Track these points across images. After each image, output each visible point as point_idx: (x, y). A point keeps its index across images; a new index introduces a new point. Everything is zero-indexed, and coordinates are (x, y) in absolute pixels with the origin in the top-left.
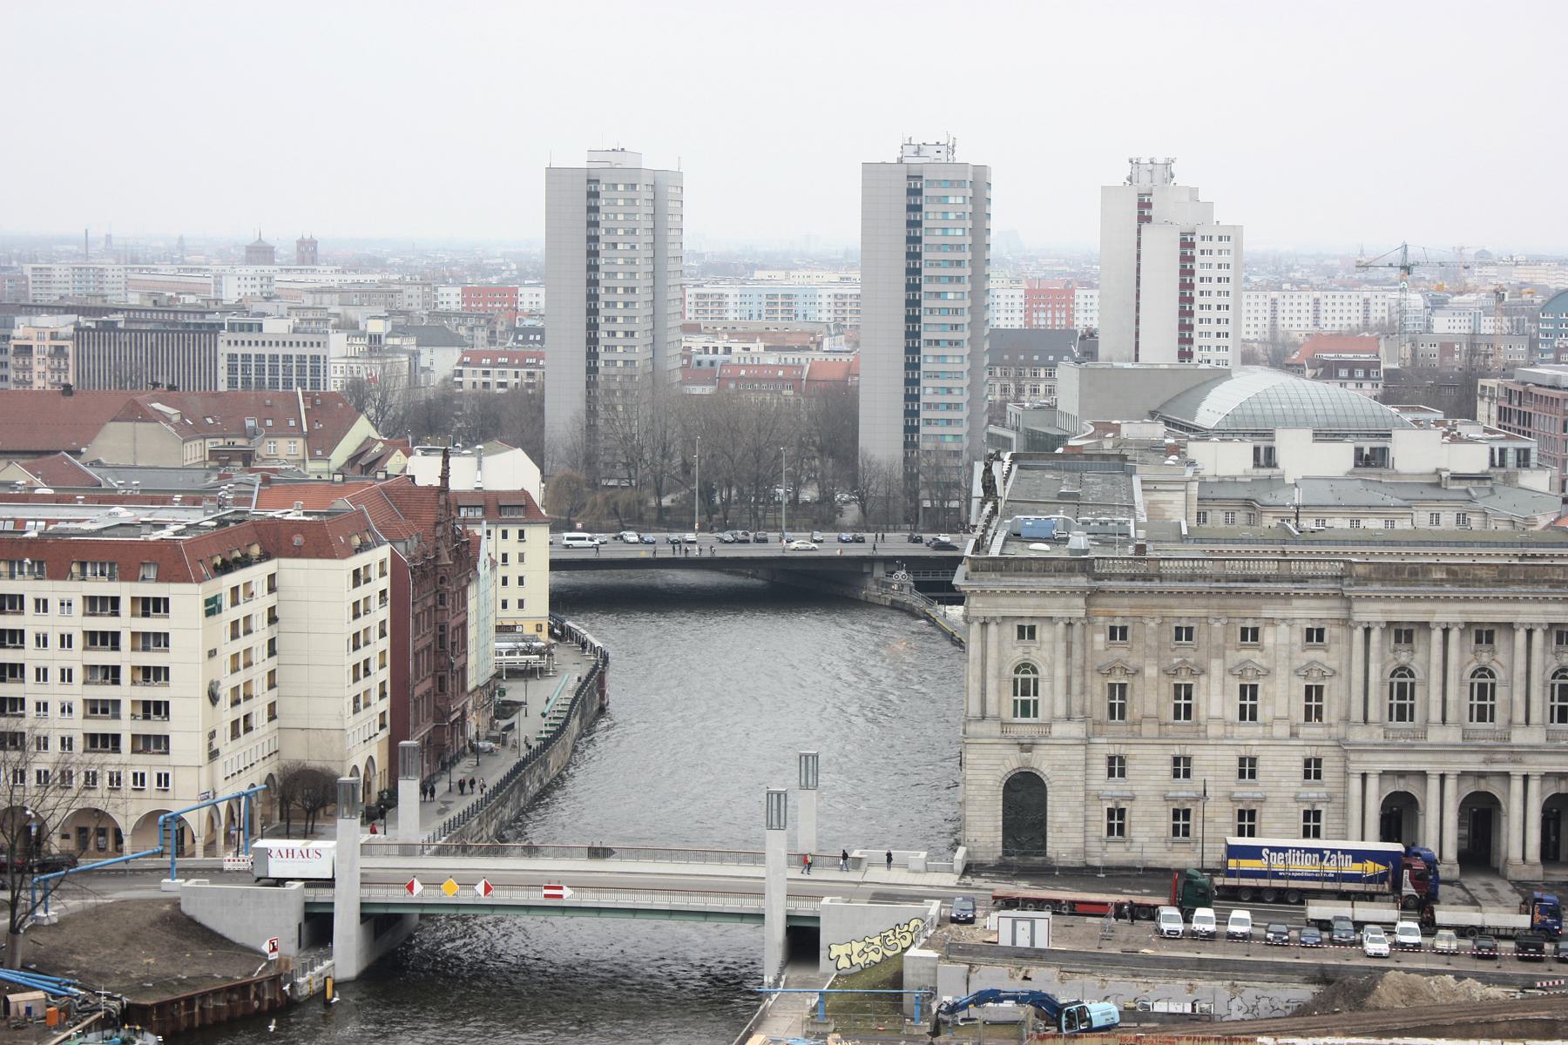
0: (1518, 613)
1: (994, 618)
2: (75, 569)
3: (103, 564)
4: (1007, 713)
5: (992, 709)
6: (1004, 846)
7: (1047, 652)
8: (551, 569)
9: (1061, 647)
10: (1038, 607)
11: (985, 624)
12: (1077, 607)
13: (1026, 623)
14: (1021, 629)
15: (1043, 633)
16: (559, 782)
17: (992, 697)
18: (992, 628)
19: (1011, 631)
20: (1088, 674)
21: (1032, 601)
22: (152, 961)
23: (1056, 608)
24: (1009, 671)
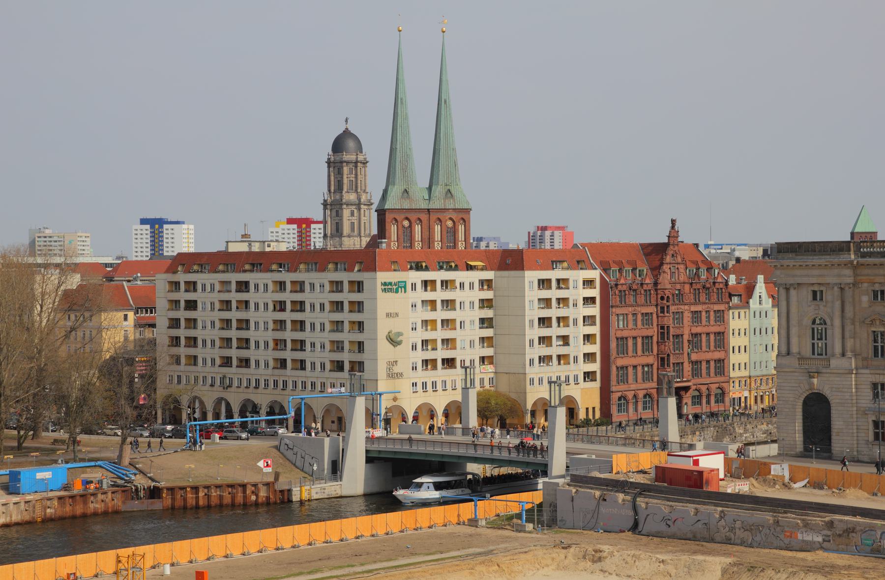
0: (794, 276)
1: (792, 285)
2: (331, 266)
3: (316, 264)
4: (807, 352)
5: (794, 349)
6: (805, 442)
7: (830, 308)
8: (197, 573)
9: (838, 304)
10: (820, 276)
11: (787, 290)
12: (847, 277)
13: (816, 288)
14: (814, 293)
15: (828, 296)
16: (406, 114)
17: (794, 340)
18: (793, 292)
19: (807, 294)
20: (857, 324)
21: (816, 272)
22: (193, 466)
23: (831, 277)
24: (807, 321)
